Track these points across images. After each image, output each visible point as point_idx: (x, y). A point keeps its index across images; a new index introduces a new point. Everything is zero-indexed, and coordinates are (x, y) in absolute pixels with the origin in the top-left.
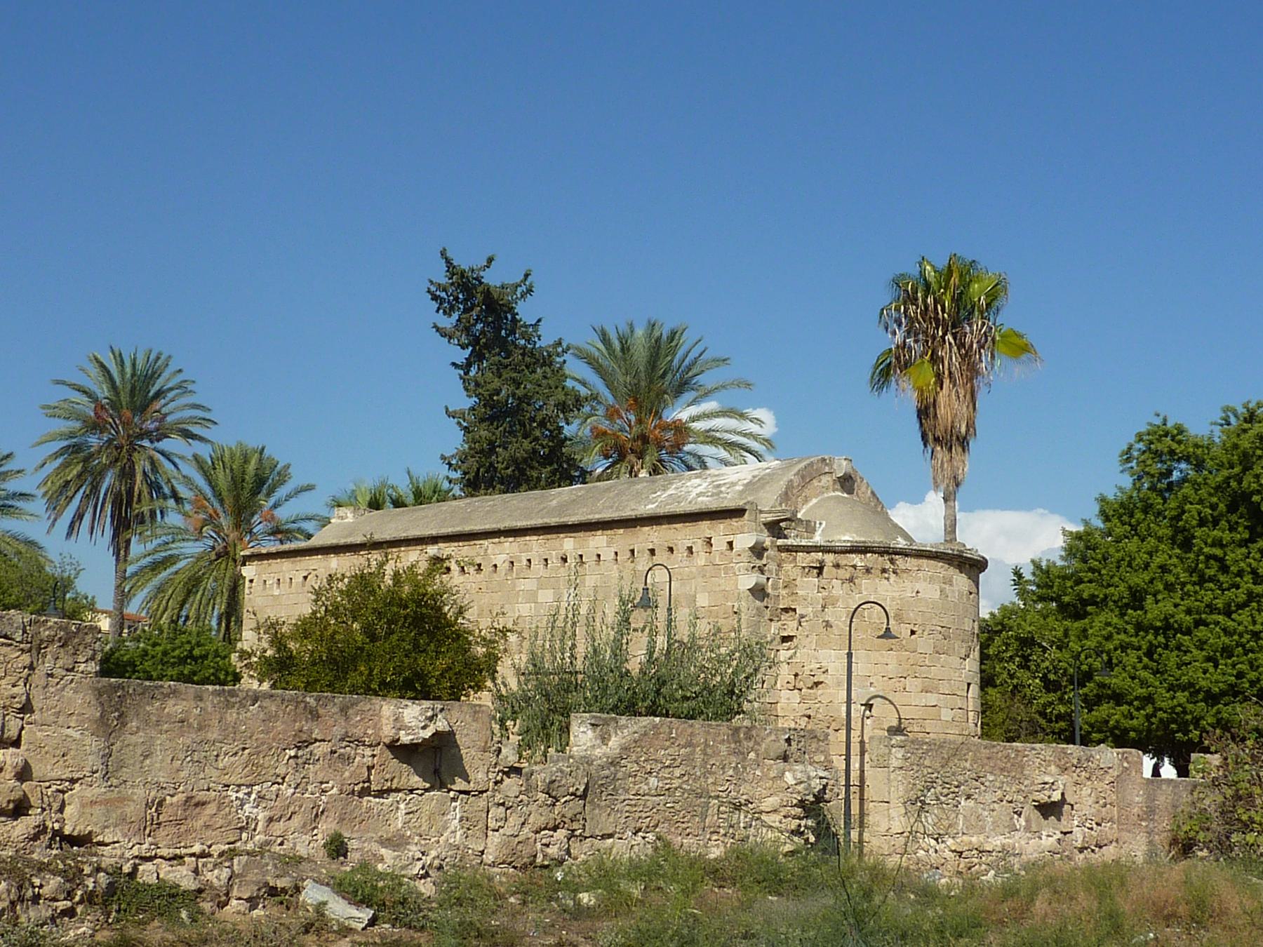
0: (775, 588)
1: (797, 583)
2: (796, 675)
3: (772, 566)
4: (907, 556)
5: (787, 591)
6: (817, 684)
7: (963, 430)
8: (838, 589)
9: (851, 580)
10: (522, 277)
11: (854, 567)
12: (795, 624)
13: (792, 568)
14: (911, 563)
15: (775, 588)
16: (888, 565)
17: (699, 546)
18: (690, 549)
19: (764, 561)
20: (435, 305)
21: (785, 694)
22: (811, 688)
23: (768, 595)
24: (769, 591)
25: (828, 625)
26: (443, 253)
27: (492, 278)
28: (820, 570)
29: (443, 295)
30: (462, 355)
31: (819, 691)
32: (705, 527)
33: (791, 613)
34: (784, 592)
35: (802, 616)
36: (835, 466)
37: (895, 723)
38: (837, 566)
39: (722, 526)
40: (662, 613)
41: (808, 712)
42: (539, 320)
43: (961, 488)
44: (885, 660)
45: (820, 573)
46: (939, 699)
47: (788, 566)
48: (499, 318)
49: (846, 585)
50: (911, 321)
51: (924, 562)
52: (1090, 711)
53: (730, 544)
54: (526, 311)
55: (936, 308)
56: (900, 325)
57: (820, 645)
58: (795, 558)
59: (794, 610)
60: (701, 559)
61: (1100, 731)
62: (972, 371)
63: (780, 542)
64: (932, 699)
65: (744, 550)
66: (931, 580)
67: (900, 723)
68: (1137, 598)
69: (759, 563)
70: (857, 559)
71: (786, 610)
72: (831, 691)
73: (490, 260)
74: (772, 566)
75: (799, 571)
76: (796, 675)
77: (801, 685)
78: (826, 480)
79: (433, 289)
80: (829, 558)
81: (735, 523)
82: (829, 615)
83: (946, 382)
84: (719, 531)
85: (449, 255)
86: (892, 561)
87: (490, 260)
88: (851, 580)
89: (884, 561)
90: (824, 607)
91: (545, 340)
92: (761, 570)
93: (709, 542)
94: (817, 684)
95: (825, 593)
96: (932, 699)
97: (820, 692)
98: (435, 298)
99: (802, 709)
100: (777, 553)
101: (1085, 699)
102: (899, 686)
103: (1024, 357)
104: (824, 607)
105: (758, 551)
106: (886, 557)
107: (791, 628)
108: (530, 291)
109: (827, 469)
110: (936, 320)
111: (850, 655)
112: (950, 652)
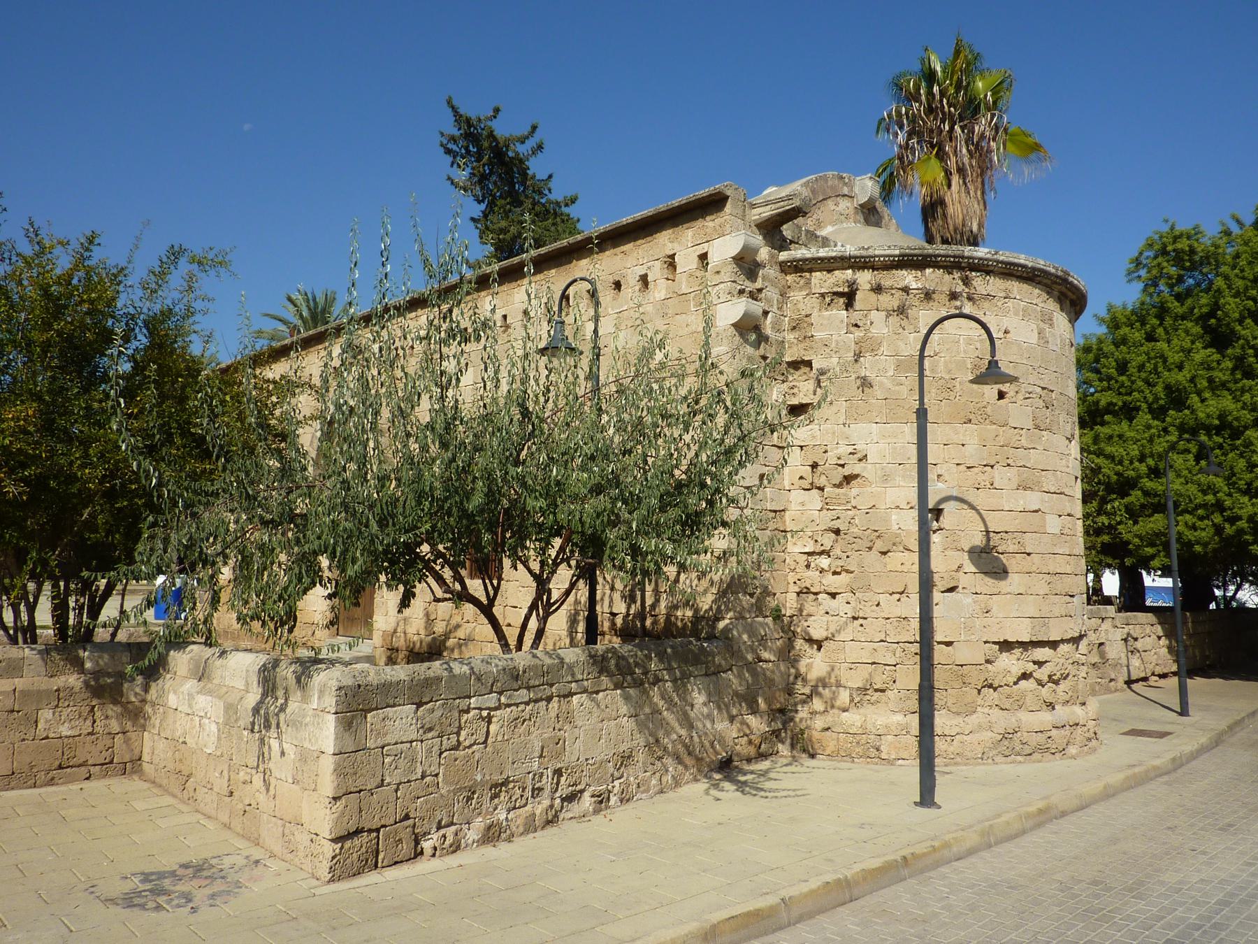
0: (777, 328)
1: (813, 319)
2: (814, 466)
3: (771, 293)
4: (988, 273)
5: (796, 334)
6: (848, 479)
7: (975, 228)
8: (879, 325)
9: (901, 311)
10: (529, 129)
11: (906, 290)
12: (811, 385)
13: (804, 297)
14: (994, 285)
15: (777, 328)
16: (960, 287)
17: (657, 272)
18: (644, 279)
19: (759, 284)
20: (449, 159)
21: (797, 496)
22: (839, 486)
23: (766, 339)
24: (768, 330)
25: (865, 383)
26: (449, 102)
27: (502, 129)
28: (849, 298)
29: (455, 148)
30: (477, 210)
31: (853, 490)
32: (665, 241)
33: (805, 369)
34: (790, 337)
35: (822, 372)
36: (856, 189)
37: (979, 540)
38: (878, 289)
39: (690, 233)
40: (585, 363)
41: (836, 524)
42: (550, 176)
43: (551, 831)
44: (961, 439)
45: (849, 305)
46: (1043, 501)
47: (797, 296)
48: (509, 172)
49: (894, 319)
50: (913, 120)
51: (1015, 287)
52: (1136, 522)
53: (703, 257)
54: (537, 168)
55: (941, 101)
56: (901, 128)
57: (853, 416)
58: (808, 283)
59: (809, 364)
60: (659, 290)
61: (1152, 545)
62: (984, 167)
63: (784, 256)
64: (1033, 500)
65: (724, 263)
66: (1026, 314)
67: (988, 540)
68: (1177, 398)
69: (750, 286)
70: (909, 278)
71: (795, 365)
72: (873, 489)
73: (497, 110)
74: (771, 293)
75: (815, 301)
76: (814, 466)
77: (822, 481)
78: (844, 205)
79: (445, 142)
80: (865, 278)
81: (710, 223)
82: (867, 367)
83: (955, 179)
84: (681, 243)
85: (454, 103)
86: (966, 281)
87: (497, 110)
88: (901, 311)
89: (952, 281)
90: (858, 356)
91: (557, 193)
92: (754, 296)
93: (671, 262)
94: (848, 479)
95: (858, 333)
96: (1033, 500)
97: (854, 491)
98: (448, 151)
99: (825, 520)
100: (780, 276)
101: (1128, 509)
102: (984, 479)
103: (1033, 156)
104: (858, 356)
105: (746, 264)
106: (957, 275)
107: (804, 391)
108: (540, 147)
109: (846, 191)
110: (944, 113)
111: (922, 414)
112: (1054, 428)
